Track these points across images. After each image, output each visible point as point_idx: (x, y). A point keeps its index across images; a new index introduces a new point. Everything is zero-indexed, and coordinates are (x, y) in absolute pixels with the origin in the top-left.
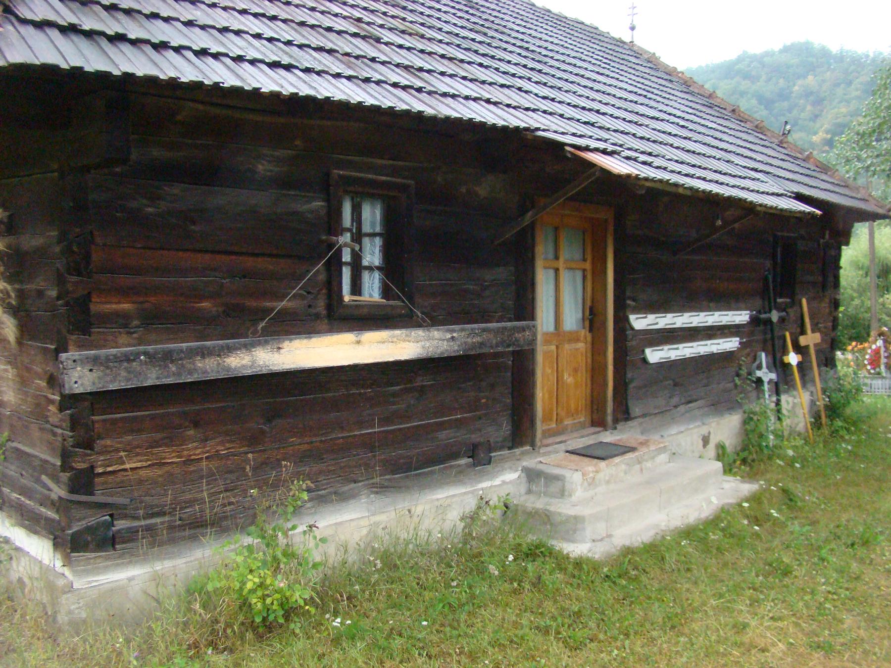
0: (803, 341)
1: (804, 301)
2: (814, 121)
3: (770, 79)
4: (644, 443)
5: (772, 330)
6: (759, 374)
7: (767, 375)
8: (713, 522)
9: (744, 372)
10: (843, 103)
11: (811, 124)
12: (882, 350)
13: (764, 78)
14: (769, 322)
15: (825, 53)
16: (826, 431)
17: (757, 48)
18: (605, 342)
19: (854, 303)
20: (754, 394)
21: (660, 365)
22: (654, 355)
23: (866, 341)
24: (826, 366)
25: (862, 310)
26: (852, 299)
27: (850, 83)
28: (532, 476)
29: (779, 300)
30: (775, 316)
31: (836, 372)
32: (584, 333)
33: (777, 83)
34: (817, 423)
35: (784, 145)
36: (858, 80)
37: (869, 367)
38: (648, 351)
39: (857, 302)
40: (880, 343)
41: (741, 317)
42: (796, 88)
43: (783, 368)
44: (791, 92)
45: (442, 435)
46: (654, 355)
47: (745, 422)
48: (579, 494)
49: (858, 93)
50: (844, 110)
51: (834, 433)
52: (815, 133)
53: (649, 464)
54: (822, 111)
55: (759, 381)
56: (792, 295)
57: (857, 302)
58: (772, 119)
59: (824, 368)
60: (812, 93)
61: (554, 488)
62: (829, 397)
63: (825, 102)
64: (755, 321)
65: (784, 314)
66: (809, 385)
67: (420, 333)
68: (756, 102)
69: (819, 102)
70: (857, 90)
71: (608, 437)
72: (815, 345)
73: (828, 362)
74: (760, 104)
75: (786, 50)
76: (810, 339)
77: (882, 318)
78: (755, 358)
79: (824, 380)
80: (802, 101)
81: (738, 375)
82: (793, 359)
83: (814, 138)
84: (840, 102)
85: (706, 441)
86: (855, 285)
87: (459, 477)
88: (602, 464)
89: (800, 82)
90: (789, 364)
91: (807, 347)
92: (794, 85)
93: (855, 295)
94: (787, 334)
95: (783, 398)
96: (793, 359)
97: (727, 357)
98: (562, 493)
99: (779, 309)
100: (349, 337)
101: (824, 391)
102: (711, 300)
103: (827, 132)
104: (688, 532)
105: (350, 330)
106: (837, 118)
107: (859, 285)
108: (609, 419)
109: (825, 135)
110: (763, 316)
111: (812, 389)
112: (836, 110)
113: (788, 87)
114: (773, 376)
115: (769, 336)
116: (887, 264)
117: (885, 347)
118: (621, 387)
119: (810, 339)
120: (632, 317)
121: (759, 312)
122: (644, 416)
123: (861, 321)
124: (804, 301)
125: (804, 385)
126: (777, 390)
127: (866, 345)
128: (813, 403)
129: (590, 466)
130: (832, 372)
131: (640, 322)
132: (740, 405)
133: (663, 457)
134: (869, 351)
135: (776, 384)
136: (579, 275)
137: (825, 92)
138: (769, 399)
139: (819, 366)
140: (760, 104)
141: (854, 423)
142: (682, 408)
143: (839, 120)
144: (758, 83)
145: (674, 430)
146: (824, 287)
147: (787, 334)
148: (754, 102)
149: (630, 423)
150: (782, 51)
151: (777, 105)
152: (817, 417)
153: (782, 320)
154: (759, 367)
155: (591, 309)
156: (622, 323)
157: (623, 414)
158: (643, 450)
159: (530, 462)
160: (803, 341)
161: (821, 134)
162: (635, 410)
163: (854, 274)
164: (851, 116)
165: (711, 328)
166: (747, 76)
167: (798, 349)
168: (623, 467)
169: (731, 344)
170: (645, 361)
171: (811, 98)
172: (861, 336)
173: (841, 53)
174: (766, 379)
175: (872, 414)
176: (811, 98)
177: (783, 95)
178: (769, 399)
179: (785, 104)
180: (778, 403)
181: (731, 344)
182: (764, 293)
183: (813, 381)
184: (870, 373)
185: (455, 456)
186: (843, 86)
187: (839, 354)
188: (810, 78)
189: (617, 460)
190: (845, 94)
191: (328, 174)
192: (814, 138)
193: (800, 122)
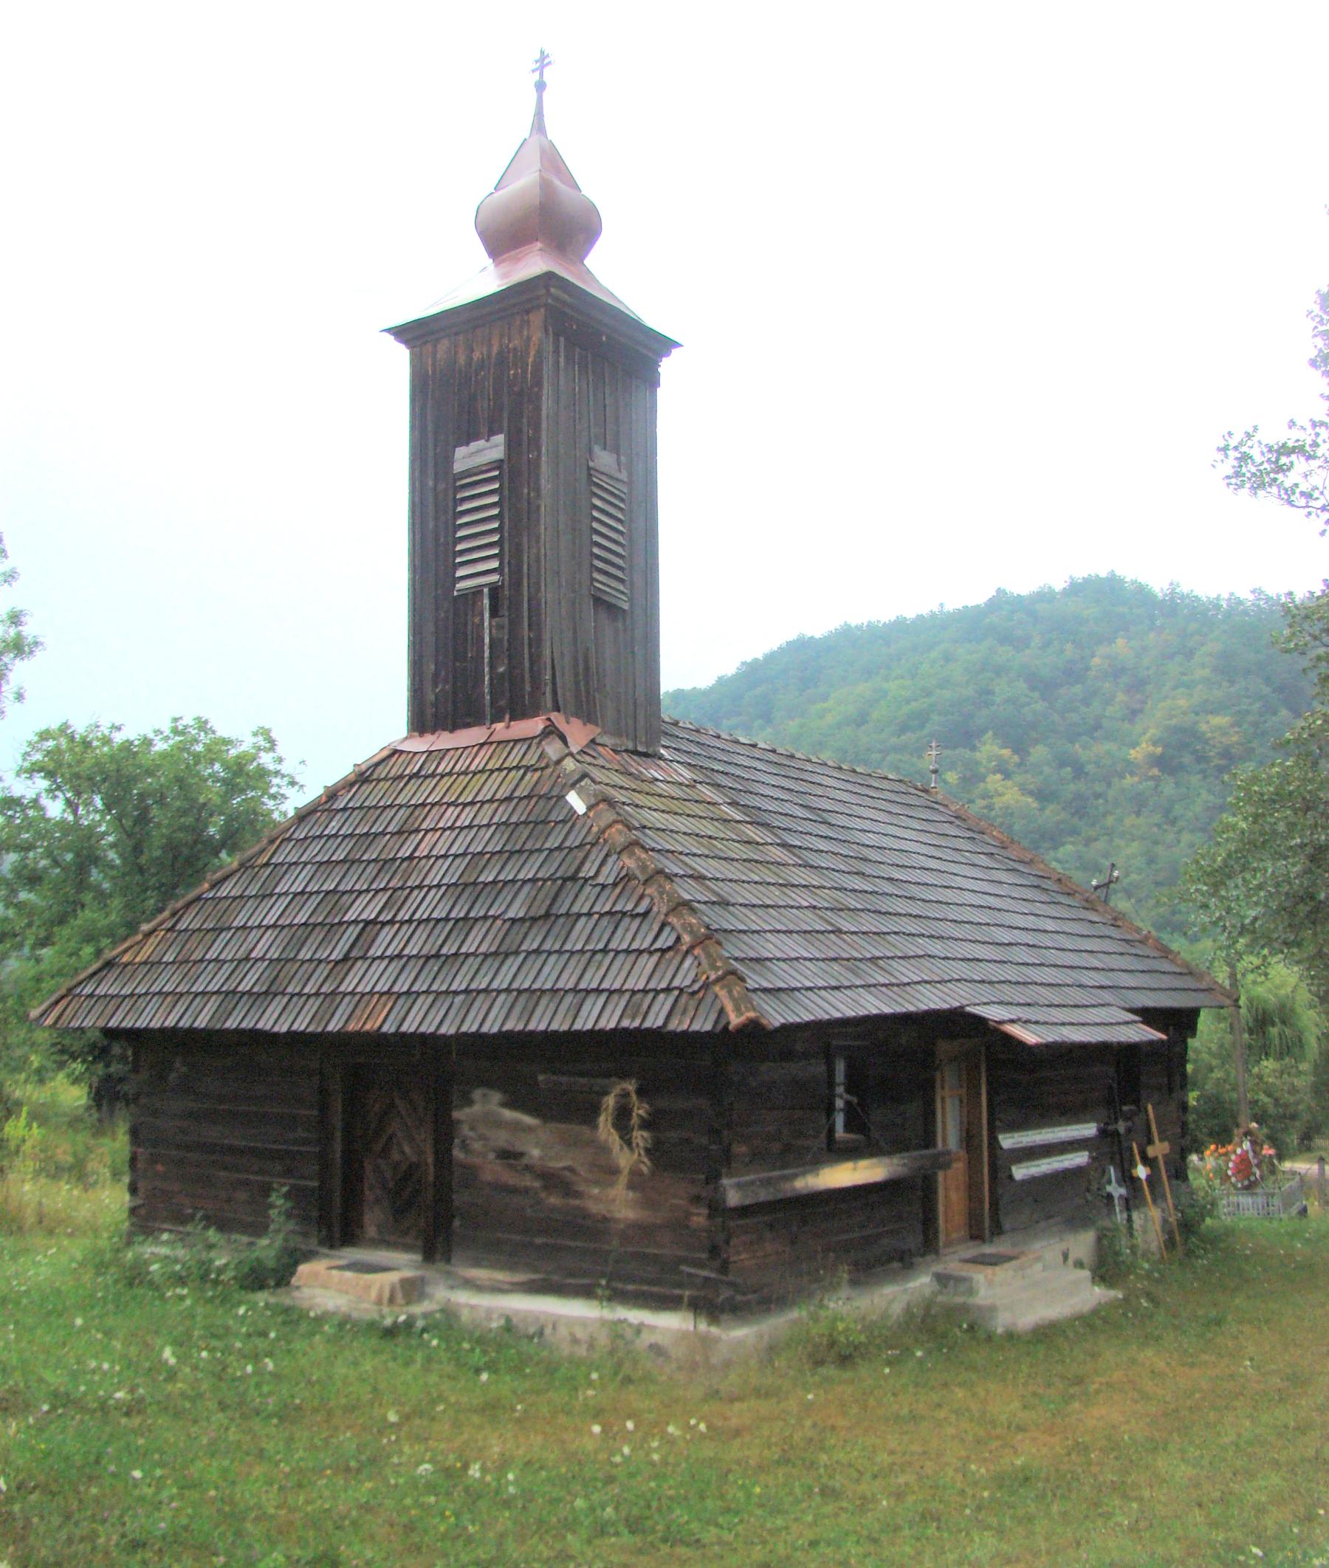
0: (1151, 1151)
1: (1150, 1107)
2: (1131, 721)
3: (1046, 644)
4: (1023, 1253)
5: (1120, 1142)
6: (1109, 1189)
7: (1117, 1190)
8: (1095, 1312)
9: (1094, 1186)
10: (1180, 690)
11: (1126, 726)
12: (1251, 1155)
13: (1036, 641)
14: (1117, 1133)
15: (1141, 592)
16: (1180, 1250)
17: (1023, 585)
18: (981, 1162)
19: (1213, 1075)
20: (1105, 1211)
21: (1023, 1182)
22: (1020, 1172)
23: (1230, 1142)
24: (1177, 1178)
25: (1228, 1087)
26: (1211, 1069)
27: (1190, 654)
28: (942, 1279)
29: (1125, 1108)
30: (1121, 1127)
31: (1188, 1186)
32: (963, 1153)
33: (1062, 651)
34: (1170, 1244)
35: (1120, 923)
36: (1204, 649)
37: (1233, 1179)
38: (1014, 1168)
39: (1217, 1074)
40: (1246, 1145)
41: (1088, 1130)
42: (1096, 661)
43: (1128, 1179)
44: (1088, 669)
45: (885, 1241)
46: (1020, 1172)
47: (1099, 1240)
48: (982, 1292)
49: (1207, 672)
50: (1183, 703)
51: (1189, 1253)
52: (1134, 745)
53: (1029, 1271)
54: (1144, 702)
55: (1110, 1196)
56: (1136, 1102)
57: (1217, 1074)
58: (1056, 717)
59: (1174, 1182)
60: (1123, 670)
61: (962, 1288)
62: (1182, 1212)
63: (1149, 687)
64: (1103, 1133)
65: (1129, 1123)
66: (1159, 1201)
67: (886, 1160)
68: (1025, 686)
69: (1138, 685)
70: (1203, 665)
71: (988, 1249)
72: (1165, 1156)
73: (1179, 1172)
74: (1032, 689)
75: (1076, 589)
76: (1159, 1149)
77: (1257, 1101)
78: (1104, 1172)
79: (1176, 1196)
80: (1107, 685)
81: (1088, 1190)
82: (1141, 1172)
83: (1133, 754)
84: (1175, 688)
85: (1065, 1256)
86: (1214, 1047)
87: (893, 1277)
88: (997, 1269)
89: (1102, 650)
90: (1139, 1179)
91: (1156, 1158)
92: (1093, 656)
93: (1214, 1062)
94: (1135, 1145)
95: (1135, 1215)
96: (1141, 1172)
97: (1078, 1172)
98: (971, 1292)
99: (1127, 1119)
100: (849, 1165)
101: (1176, 1207)
102: (1063, 1114)
103: (1155, 744)
104: (1080, 1318)
105: (848, 1159)
106: (1171, 717)
107: (1221, 1046)
108: (987, 1232)
109: (1151, 748)
110: (1110, 1128)
111: (1164, 1206)
112: (1169, 702)
113: (1082, 658)
114: (1123, 1191)
115: (1115, 1148)
116: (1264, 1012)
117: (1254, 1152)
118: (994, 1204)
119: (1159, 1149)
120: (1001, 1137)
121: (1106, 1124)
122: (1014, 1230)
123: (1227, 1106)
124: (1150, 1107)
125: (1154, 1201)
126: (1128, 1205)
127: (1230, 1148)
128: (1165, 1221)
129: (989, 1270)
130: (1183, 1186)
131: (1008, 1141)
132: (1094, 1223)
133: (1039, 1266)
134: (1233, 1157)
135: (1127, 1200)
136: (957, 1103)
137: (1148, 669)
138: (1120, 1217)
139: (1169, 1177)
140: (1032, 689)
141: (1213, 1241)
142: (1042, 1224)
143: (1174, 722)
144: (1027, 651)
145: (1037, 1245)
146: (1171, 1090)
147: (1135, 1145)
148: (1022, 685)
149: (1003, 1237)
150: (1065, 593)
151: (1062, 691)
152: (1170, 1234)
153: (1129, 1130)
154: (1109, 1182)
155: (968, 1131)
156: (993, 1142)
157: (997, 1230)
158: (1023, 1260)
159: (938, 1268)
160: (1151, 1151)
161: (1144, 745)
162: (1007, 1225)
163: (1213, 1027)
164: (1197, 714)
165: (1063, 1143)
166: (1005, 639)
167: (1146, 1161)
168: (1011, 1273)
169: (1080, 1158)
170: (1011, 1177)
171: (1124, 680)
172: (1223, 1136)
173: (1172, 599)
174: (1116, 1195)
175: (1229, 1232)
176: (1124, 680)
177: (1073, 673)
178: (1120, 1217)
179: (1078, 689)
180: (1129, 1220)
181: (1080, 1158)
182: (1109, 1103)
183: (1164, 1197)
184: (1236, 1189)
185: (890, 1260)
186: (1179, 658)
187: (1194, 1158)
188: (1120, 642)
189: (1006, 1266)
190: (1184, 674)
191: (829, 1044)
192: (1133, 754)
193: (1105, 723)
